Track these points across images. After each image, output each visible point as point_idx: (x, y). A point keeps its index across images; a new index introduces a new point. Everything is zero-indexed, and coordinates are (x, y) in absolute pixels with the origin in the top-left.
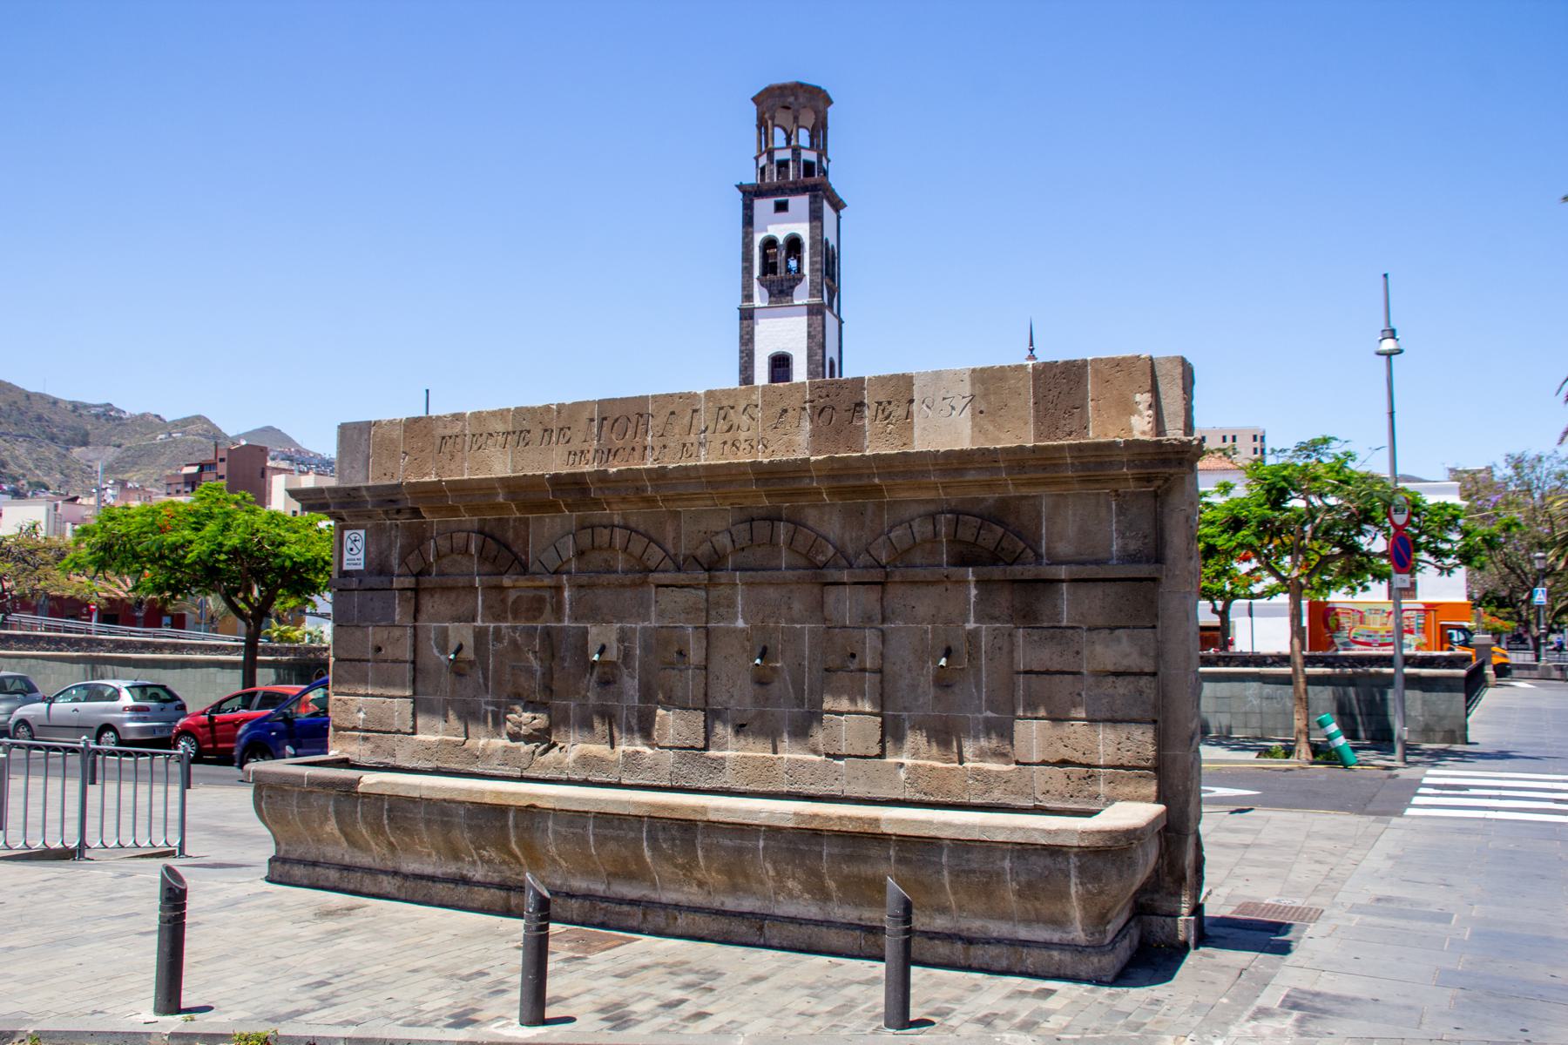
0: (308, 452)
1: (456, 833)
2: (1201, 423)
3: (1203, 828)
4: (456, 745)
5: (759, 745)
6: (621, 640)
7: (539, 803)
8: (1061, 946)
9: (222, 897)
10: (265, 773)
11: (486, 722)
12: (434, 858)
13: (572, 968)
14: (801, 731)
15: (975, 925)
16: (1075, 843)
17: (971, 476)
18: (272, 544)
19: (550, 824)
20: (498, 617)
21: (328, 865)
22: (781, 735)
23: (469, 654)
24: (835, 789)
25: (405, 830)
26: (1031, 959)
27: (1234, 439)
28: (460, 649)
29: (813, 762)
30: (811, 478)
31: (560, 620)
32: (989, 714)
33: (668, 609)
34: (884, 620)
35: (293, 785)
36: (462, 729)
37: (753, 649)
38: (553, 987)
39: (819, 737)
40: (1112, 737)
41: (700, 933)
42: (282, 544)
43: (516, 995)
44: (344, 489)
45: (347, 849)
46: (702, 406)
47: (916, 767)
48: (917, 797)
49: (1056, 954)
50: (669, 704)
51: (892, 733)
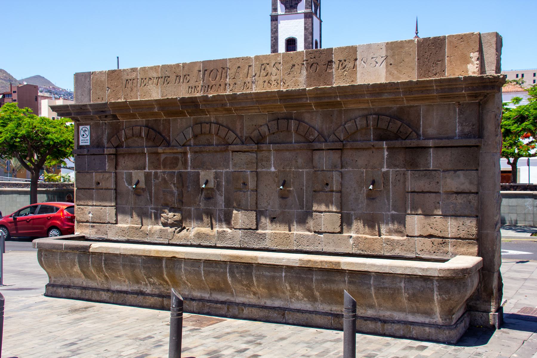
0: (59, 88)
1: (137, 271)
2: (505, 68)
3: (502, 269)
4: (137, 229)
5: (282, 227)
6: (216, 178)
7: (177, 256)
8: (430, 325)
9: (22, 304)
10: (44, 244)
11: (151, 218)
12: (127, 282)
13: (194, 334)
14: (302, 221)
15: (387, 314)
16: (436, 275)
17: (385, 96)
18: (43, 133)
19: (183, 265)
20: (156, 168)
21: (75, 287)
22: (293, 223)
23: (142, 185)
24: (319, 248)
25: (113, 270)
26: (415, 331)
27: (523, 75)
28: (137, 183)
29: (308, 236)
30: (307, 98)
31: (186, 169)
32: (394, 212)
33: (238, 163)
34: (342, 167)
35: (58, 249)
37: (279, 181)
38: (184, 343)
39: (311, 223)
40: (455, 224)
41: (254, 317)
42: (48, 133)
43: (167, 347)
44: (79, 105)
45: (84, 279)
46: (253, 64)
47: (358, 238)
48: (359, 252)
49: (427, 329)
50: (238, 208)
51: (346, 221)
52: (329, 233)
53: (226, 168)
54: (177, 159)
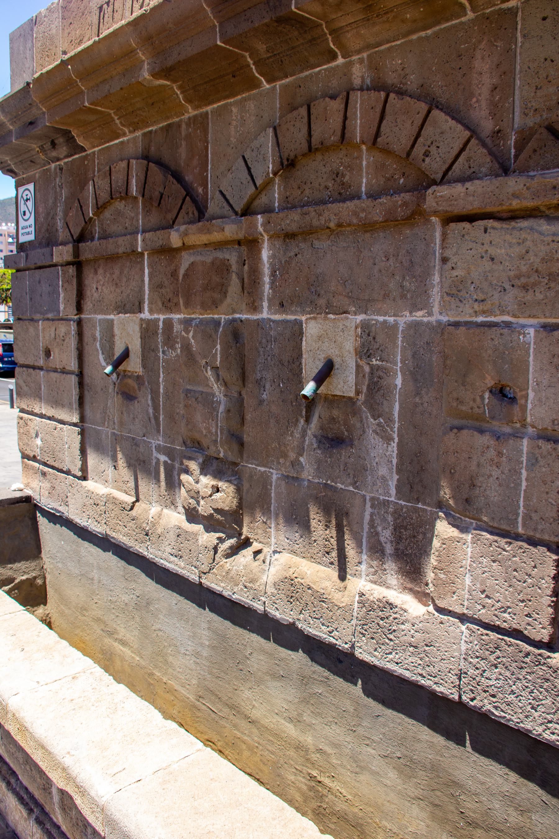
6: (365, 352)
20: (169, 305)
28: (326, 373)
31: (255, 308)
36: (132, 484)
50: (466, 515)
52: (249, 169)
53: (414, 308)
54: (223, 268)
